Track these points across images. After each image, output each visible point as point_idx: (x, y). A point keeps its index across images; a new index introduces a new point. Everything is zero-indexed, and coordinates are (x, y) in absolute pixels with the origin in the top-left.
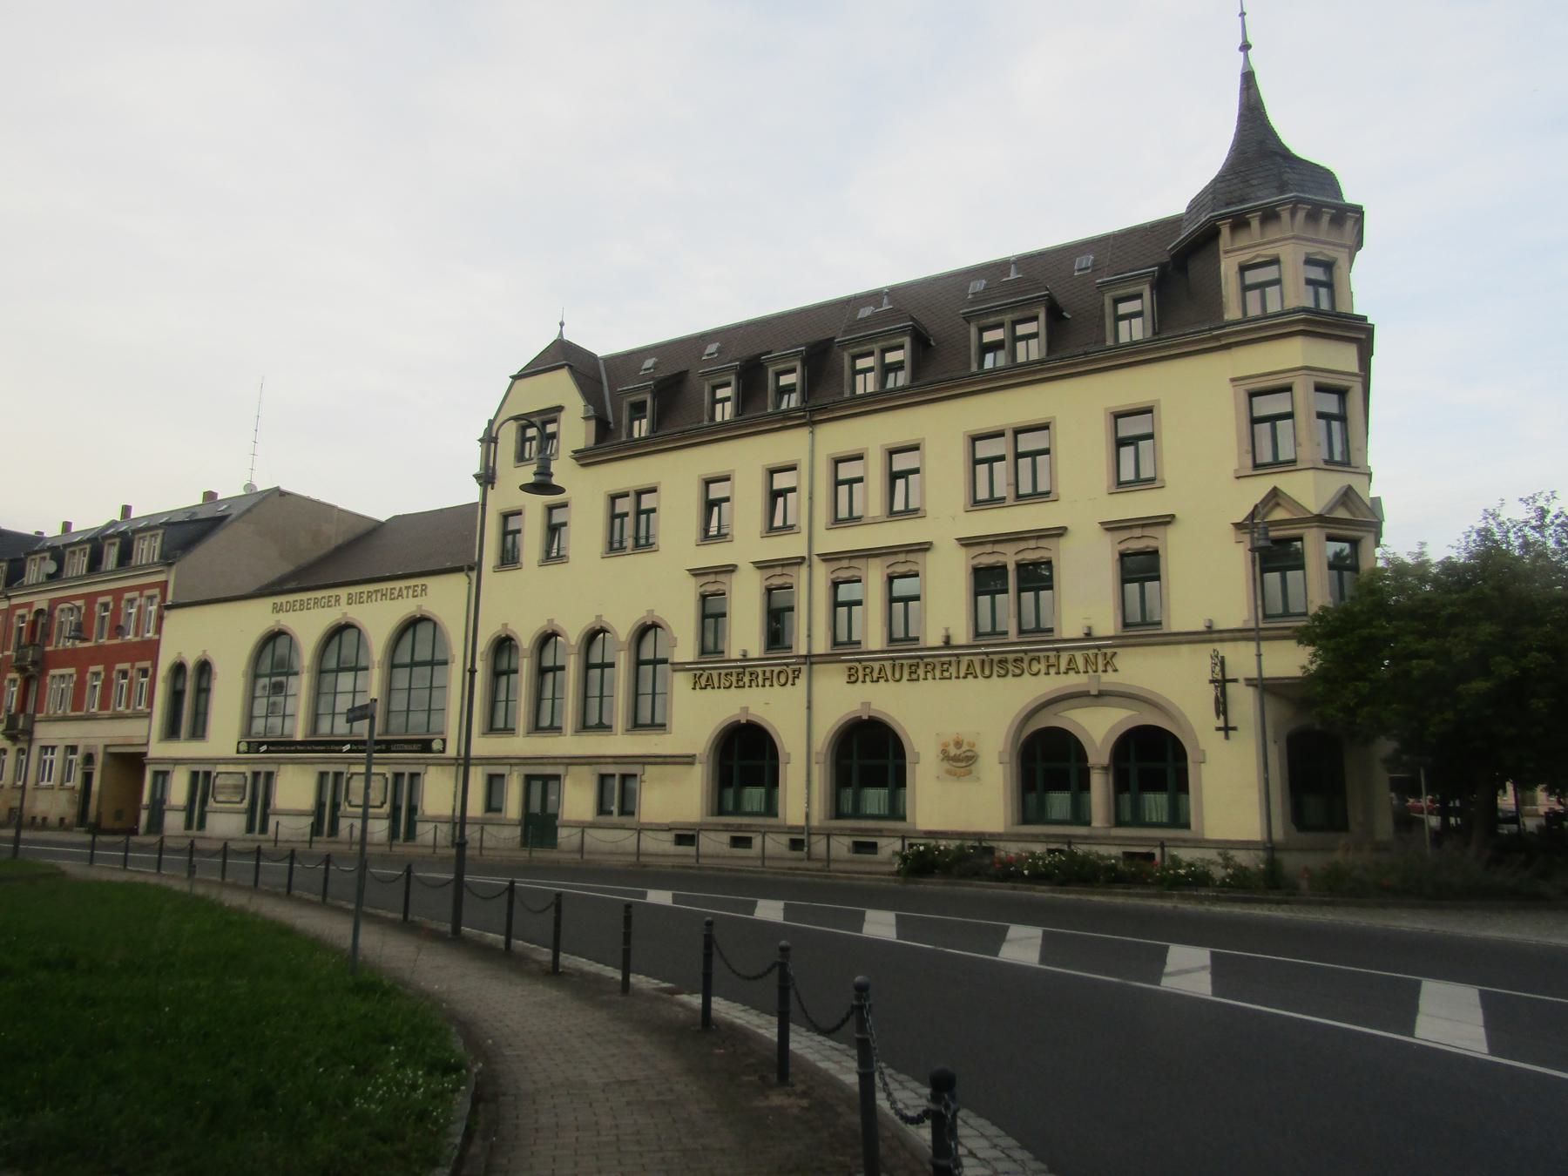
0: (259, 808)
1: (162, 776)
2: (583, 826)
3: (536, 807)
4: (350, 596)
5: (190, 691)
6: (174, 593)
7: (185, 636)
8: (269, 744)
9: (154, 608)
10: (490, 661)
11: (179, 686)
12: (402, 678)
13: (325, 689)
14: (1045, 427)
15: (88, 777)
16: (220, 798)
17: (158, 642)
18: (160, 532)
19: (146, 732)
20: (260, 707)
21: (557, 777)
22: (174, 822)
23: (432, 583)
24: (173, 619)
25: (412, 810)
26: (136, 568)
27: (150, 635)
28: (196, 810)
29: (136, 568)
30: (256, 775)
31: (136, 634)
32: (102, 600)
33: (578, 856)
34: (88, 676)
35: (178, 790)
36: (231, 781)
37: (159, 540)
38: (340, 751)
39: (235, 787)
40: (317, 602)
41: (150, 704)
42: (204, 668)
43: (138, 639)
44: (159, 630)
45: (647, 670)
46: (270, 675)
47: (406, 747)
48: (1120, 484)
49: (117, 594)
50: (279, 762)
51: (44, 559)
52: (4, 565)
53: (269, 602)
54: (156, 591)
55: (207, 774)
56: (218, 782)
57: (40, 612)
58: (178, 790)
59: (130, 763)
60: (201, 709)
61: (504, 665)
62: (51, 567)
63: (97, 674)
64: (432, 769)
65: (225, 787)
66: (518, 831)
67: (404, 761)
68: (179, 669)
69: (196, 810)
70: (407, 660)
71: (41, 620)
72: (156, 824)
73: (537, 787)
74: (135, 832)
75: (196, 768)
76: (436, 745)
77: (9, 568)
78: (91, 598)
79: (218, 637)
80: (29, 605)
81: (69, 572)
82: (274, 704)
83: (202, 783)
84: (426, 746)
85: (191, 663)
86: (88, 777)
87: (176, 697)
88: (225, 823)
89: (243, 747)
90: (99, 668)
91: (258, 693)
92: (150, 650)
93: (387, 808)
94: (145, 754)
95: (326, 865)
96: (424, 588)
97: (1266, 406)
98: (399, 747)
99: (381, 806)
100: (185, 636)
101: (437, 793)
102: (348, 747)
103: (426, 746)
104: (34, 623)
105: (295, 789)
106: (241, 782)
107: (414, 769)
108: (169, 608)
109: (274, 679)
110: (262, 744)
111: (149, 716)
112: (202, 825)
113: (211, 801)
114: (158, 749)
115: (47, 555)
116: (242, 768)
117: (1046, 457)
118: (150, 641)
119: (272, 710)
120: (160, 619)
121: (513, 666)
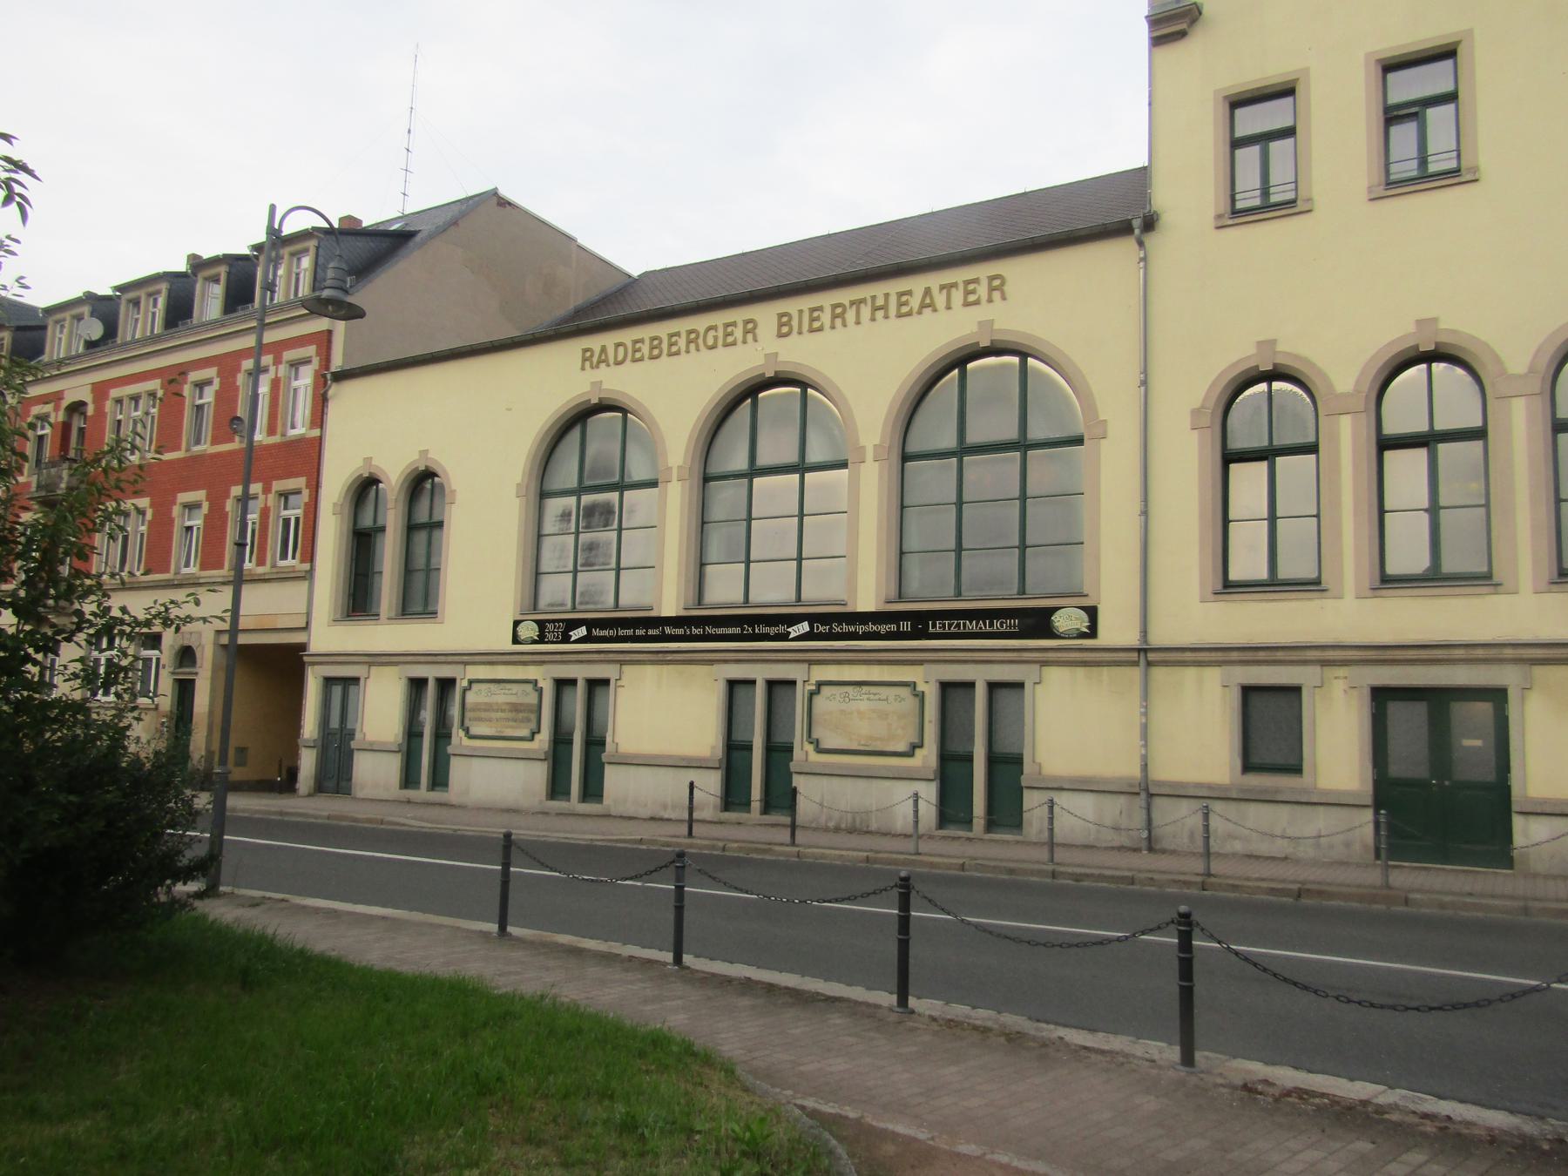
0: (578, 755)
1: (343, 687)
2: (1206, 797)
3: (335, 723)
4: (784, 322)
5: (397, 534)
6: (345, 355)
7: (372, 430)
8: (591, 624)
9: (305, 380)
10: (347, 510)
11: (367, 521)
12: (934, 480)
13: (718, 511)
14: (1286, 91)
15: (185, 689)
16: (475, 730)
17: (319, 441)
18: (312, 244)
19: (303, 606)
20: (559, 550)
21: (356, 680)
22: (375, 773)
23: (1014, 270)
24: (347, 400)
25: (595, 743)
26: (125, 345)
27: (300, 430)
28: (428, 745)
29: (125, 345)
30: (562, 684)
31: (271, 430)
32: (195, 376)
33: (1199, 866)
34: (176, 511)
35: (381, 711)
36: (502, 696)
37: (161, 301)
38: (784, 637)
39: (515, 708)
40: (693, 338)
41: (310, 556)
42: (423, 482)
43: (276, 439)
44: (319, 417)
45: (421, 537)
46: (579, 491)
47: (972, 626)
48: (1235, 213)
49: (228, 365)
50: (623, 661)
51: (79, 318)
52: (6, 336)
53: (570, 350)
54: (310, 350)
55: (446, 685)
56: (471, 698)
57: (77, 408)
58: (381, 711)
59: (275, 667)
60: (420, 562)
61: (422, 516)
62: (96, 330)
63: (192, 507)
64: (1054, 675)
65: (489, 707)
66: (1363, 824)
67: (980, 663)
68: (365, 487)
69: (428, 745)
70: (740, 463)
71: (77, 423)
72: (336, 773)
73: (337, 691)
74: (288, 783)
75: (419, 671)
76: (1067, 620)
77: (15, 341)
78: (174, 377)
79: (472, 426)
80: (57, 397)
81: (125, 333)
82: (591, 547)
83: (434, 696)
84: (1037, 623)
85: (394, 475)
86: (185, 689)
87: (362, 542)
88: (497, 778)
89: (529, 630)
90: (199, 495)
91: (550, 526)
92: (306, 457)
93: (928, 757)
94: (302, 647)
95: (741, 868)
96: (997, 286)
97: (1407, 86)
98: (950, 626)
99: (909, 754)
100: (372, 430)
101: (1073, 726)
102: (804, 627)
103: (1037, 623)
104: (66, 427)
105: (666, 715)
106: (532, 699)
107: (598, 672)
108: (341, 376)
109: (587, 499)
110: (574, 624)
111: (309, 576)
112: (439, 779)
113: (458, 735)
114: (329, 636)
115: (86, 310)
116: (531, 672)
117: (1449, 109)
118: (301, 440)
119: (587, 557)
120: (321, 403)
121: (380, 523)
